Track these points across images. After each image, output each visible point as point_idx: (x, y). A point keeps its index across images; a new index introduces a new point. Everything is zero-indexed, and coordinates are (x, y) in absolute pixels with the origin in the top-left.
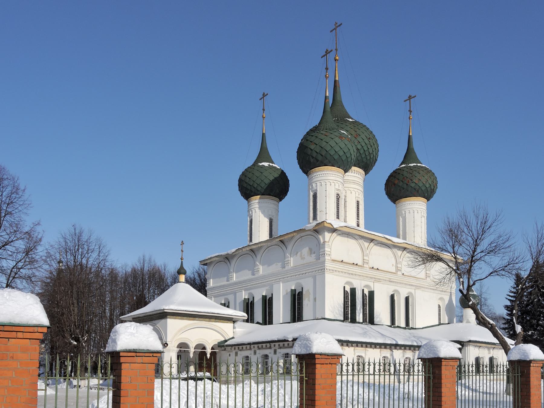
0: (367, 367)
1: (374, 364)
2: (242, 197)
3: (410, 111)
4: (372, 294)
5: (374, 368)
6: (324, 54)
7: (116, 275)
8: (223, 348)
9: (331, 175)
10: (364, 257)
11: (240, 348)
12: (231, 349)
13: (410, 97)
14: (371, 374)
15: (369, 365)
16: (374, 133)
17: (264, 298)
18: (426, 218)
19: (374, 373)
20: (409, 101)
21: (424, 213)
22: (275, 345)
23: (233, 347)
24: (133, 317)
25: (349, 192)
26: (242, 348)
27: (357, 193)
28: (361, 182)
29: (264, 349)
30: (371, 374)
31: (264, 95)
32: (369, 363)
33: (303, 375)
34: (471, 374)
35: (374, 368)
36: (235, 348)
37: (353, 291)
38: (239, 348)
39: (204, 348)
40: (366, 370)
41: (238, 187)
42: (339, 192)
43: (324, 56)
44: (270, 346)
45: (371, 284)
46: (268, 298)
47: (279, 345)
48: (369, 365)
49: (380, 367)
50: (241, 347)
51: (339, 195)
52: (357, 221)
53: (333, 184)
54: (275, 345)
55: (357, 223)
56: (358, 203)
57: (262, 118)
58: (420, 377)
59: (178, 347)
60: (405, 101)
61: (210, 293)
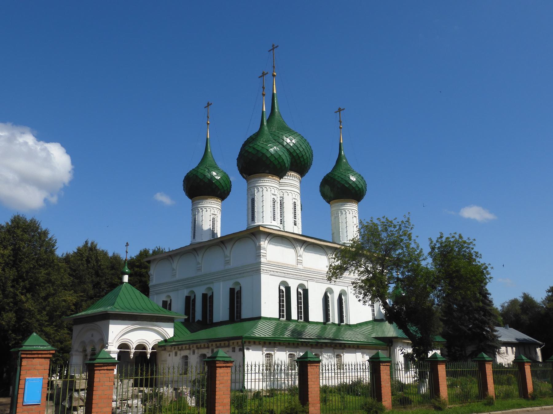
0: (253, 367)
1: (259, 366)
2: (187, 196)
3: (340, 122)
4: (306, 291)
5: (259, 368)
6: (261, 75)
7: (34, 224)
8: (163, 348)
9: (267, 182)
10: (298, 257)
11: (183, 348)
12: (171, 349)
13: (340, 110)
14: (257, 373)
15: (255, 366)
16: (308, 141)
17: (204, 296)
18: (357, 218)
19: (259, 372)
20: (338, 113)
21: (355, 214)
22: (212, 345)
23: (173, 347)
24: (74, 318)
25: (286, 194)
26: (182, 347)
27: (294, 195)
28: (298, 185)
29: (202, 348)
30: (257, 373)
31: (209, 105)
32: (247, 365)
33: (150, 377)
34: (327, 372)
35: (259, 368)
36: (175, 348)
37: (288, 289)
38: (178, 348)
39: (144, 348)
40: (253, 369)
41: (183, 187)
42: (275, 197)
43: (261, 77)
44: (208, 346)
45: (305, 283)
46: (209, 296)
47: (216, 345)
48: (255, 366)
49: (263, 368)
50: (180, 347)
51: (275, 199)
52: (294, 221)
53: (269, 190)
54: (212, 345)
55: (294, 223)
56: (295, 204)
57: (207, 125)
58: (367, 373)
59: (119, 348)
60: (336, 112)
61: (152, 290)
